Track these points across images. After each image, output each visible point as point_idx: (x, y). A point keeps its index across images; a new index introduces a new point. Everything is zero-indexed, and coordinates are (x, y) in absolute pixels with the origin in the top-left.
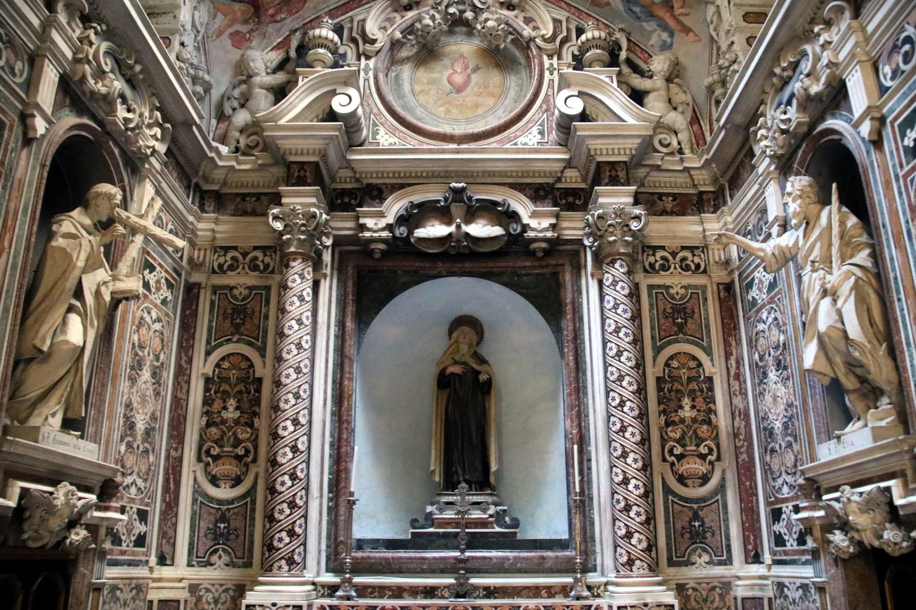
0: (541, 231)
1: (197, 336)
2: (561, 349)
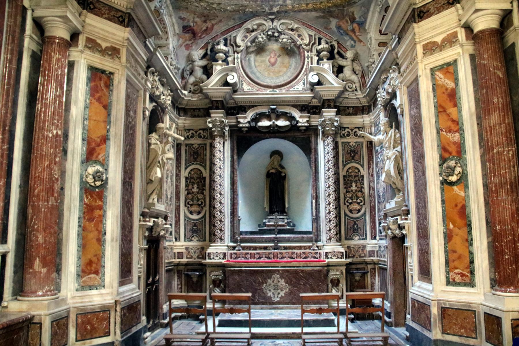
0: (304, 123)
1: (182, 162)
2: (310, 165)
